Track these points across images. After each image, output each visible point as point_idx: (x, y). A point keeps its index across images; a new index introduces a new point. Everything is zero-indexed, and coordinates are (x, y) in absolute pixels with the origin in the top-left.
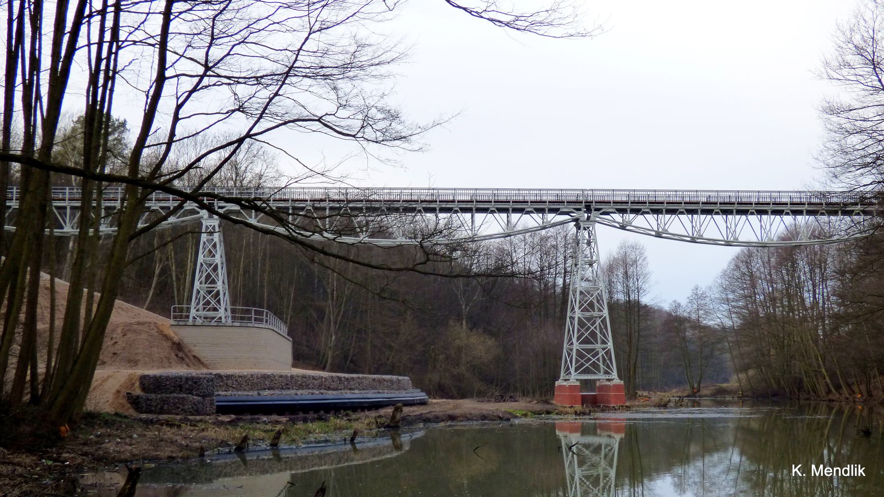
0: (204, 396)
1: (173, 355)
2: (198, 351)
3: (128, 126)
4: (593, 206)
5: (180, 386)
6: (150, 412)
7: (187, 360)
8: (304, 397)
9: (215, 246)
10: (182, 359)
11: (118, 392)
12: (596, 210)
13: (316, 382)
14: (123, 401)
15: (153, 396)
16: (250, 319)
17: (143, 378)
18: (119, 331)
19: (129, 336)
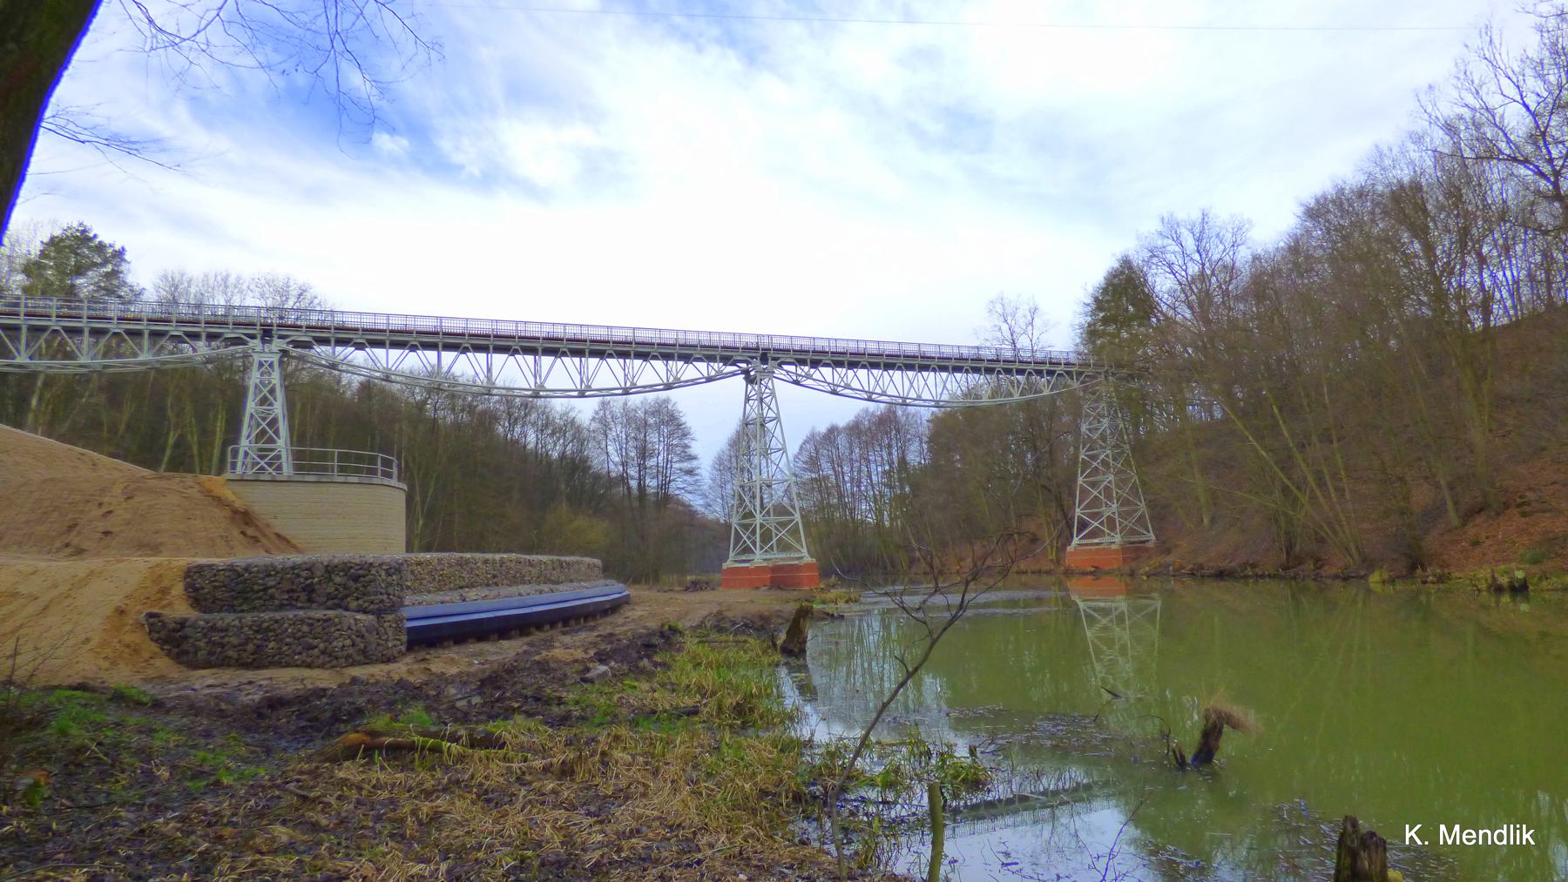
0: (379, 613)
1: (236, 532)
2: (280, 526)
3: (127, 257)
4: (771, 354)
5: (310, 590)
6: (225, 663)
7: (264, 540)
8: (485, 604)
9: (272, 391)
10: (256, 540)
11: (121, 612)
12: (775, 359)
13: (534, 571)
14: (138, 638)
15: (229, 618)
16: (373, 472)
17: (193, 576)
18: (117, 489)
19: (137, 499)
